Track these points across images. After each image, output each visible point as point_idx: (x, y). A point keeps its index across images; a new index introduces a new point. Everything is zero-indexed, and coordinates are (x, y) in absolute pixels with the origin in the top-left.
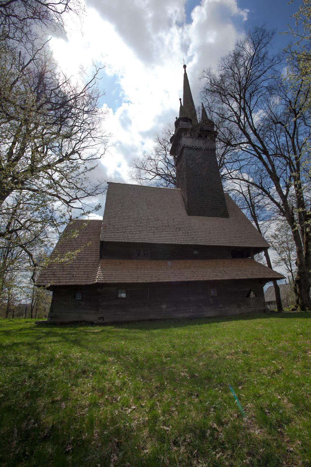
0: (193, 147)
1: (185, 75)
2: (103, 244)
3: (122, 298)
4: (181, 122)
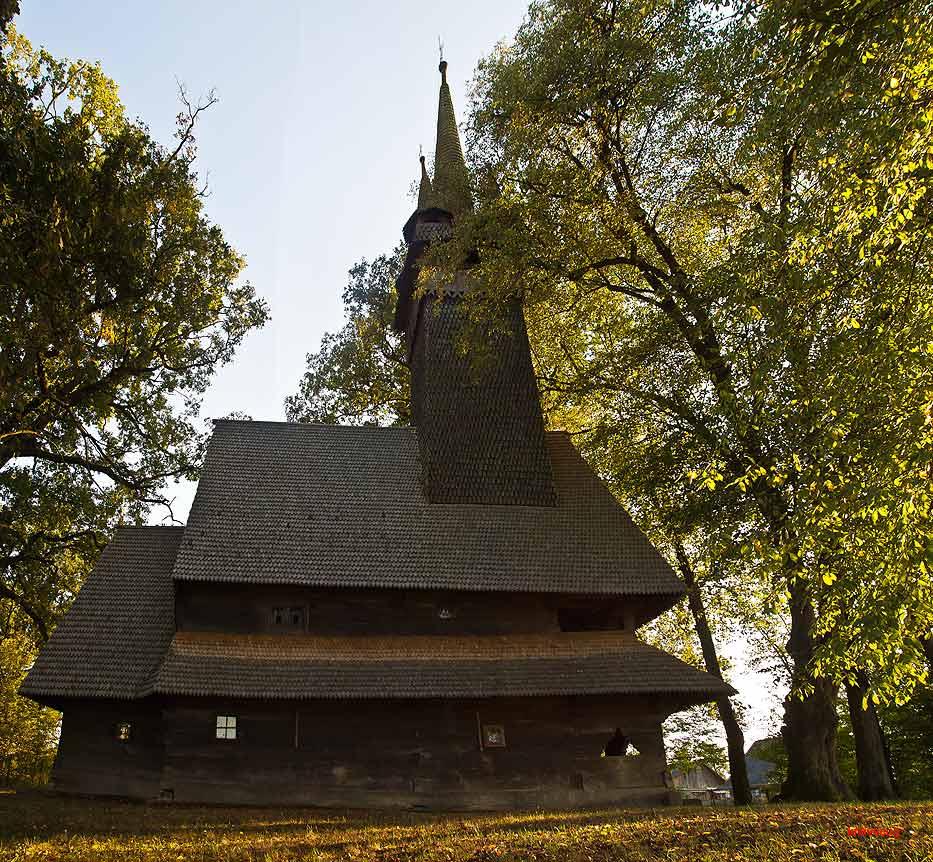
0: (454, 296)
1: (445, 90)
2: (184, 589)
3: (225, 741)
4: (419, 225)
